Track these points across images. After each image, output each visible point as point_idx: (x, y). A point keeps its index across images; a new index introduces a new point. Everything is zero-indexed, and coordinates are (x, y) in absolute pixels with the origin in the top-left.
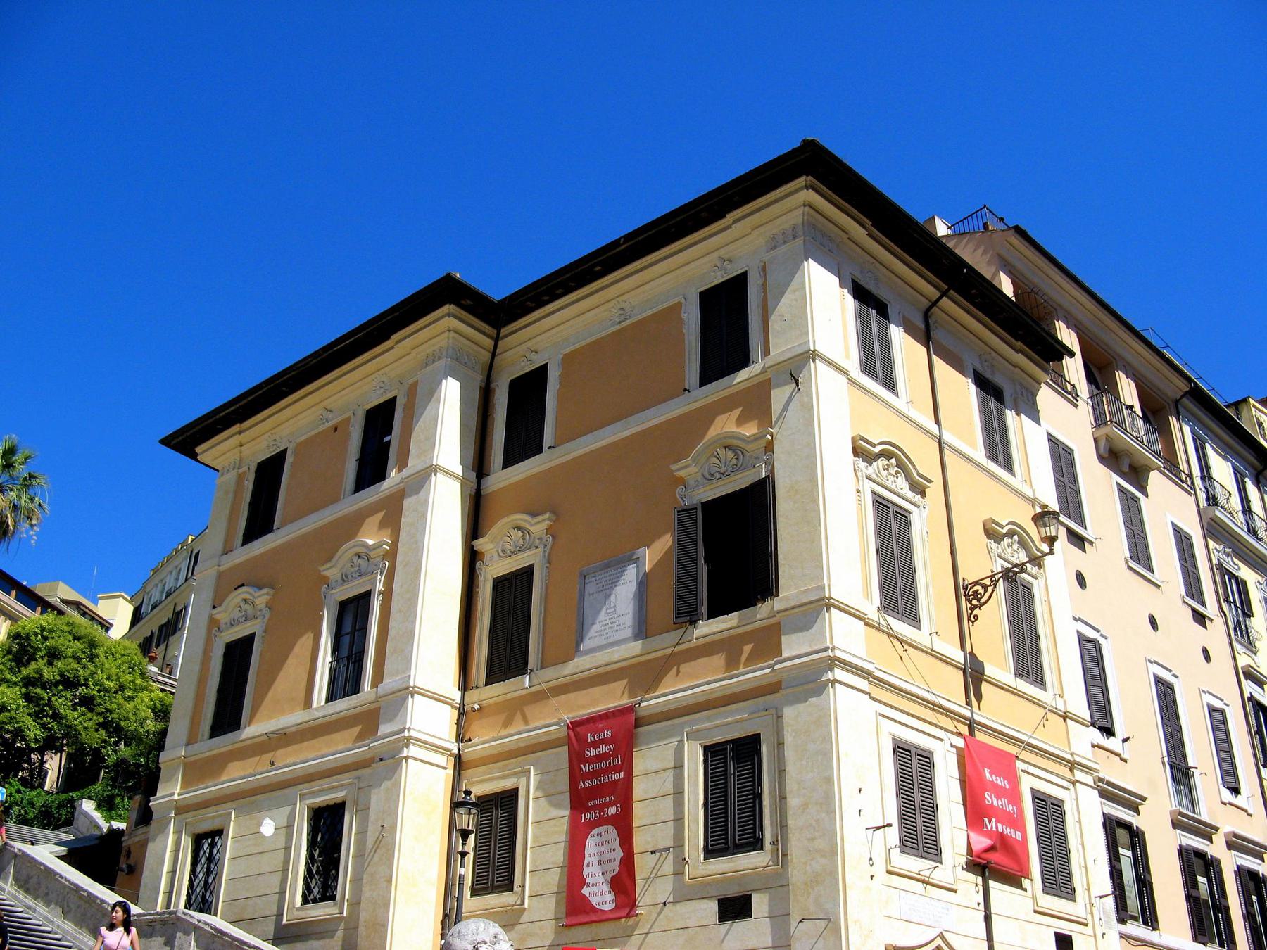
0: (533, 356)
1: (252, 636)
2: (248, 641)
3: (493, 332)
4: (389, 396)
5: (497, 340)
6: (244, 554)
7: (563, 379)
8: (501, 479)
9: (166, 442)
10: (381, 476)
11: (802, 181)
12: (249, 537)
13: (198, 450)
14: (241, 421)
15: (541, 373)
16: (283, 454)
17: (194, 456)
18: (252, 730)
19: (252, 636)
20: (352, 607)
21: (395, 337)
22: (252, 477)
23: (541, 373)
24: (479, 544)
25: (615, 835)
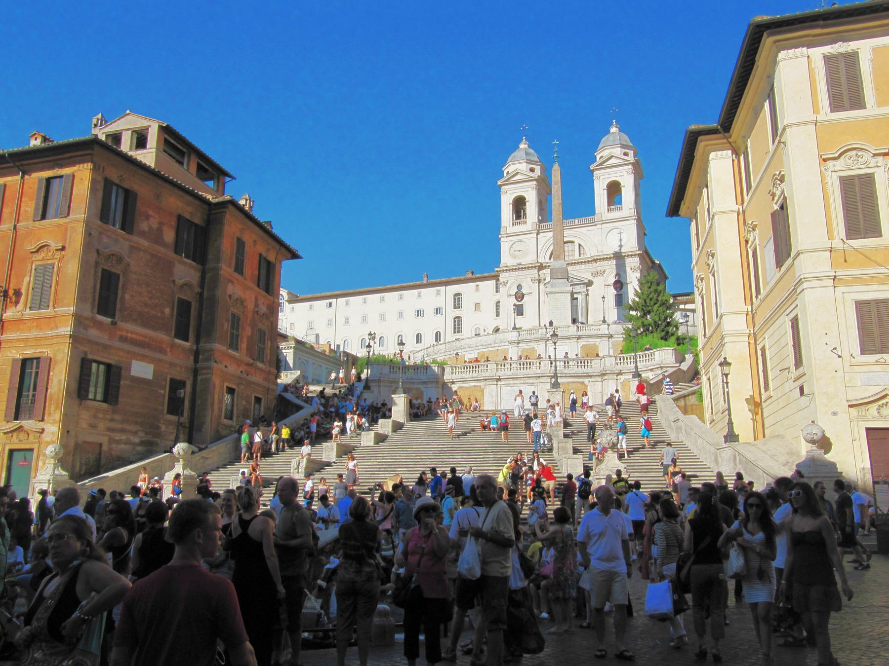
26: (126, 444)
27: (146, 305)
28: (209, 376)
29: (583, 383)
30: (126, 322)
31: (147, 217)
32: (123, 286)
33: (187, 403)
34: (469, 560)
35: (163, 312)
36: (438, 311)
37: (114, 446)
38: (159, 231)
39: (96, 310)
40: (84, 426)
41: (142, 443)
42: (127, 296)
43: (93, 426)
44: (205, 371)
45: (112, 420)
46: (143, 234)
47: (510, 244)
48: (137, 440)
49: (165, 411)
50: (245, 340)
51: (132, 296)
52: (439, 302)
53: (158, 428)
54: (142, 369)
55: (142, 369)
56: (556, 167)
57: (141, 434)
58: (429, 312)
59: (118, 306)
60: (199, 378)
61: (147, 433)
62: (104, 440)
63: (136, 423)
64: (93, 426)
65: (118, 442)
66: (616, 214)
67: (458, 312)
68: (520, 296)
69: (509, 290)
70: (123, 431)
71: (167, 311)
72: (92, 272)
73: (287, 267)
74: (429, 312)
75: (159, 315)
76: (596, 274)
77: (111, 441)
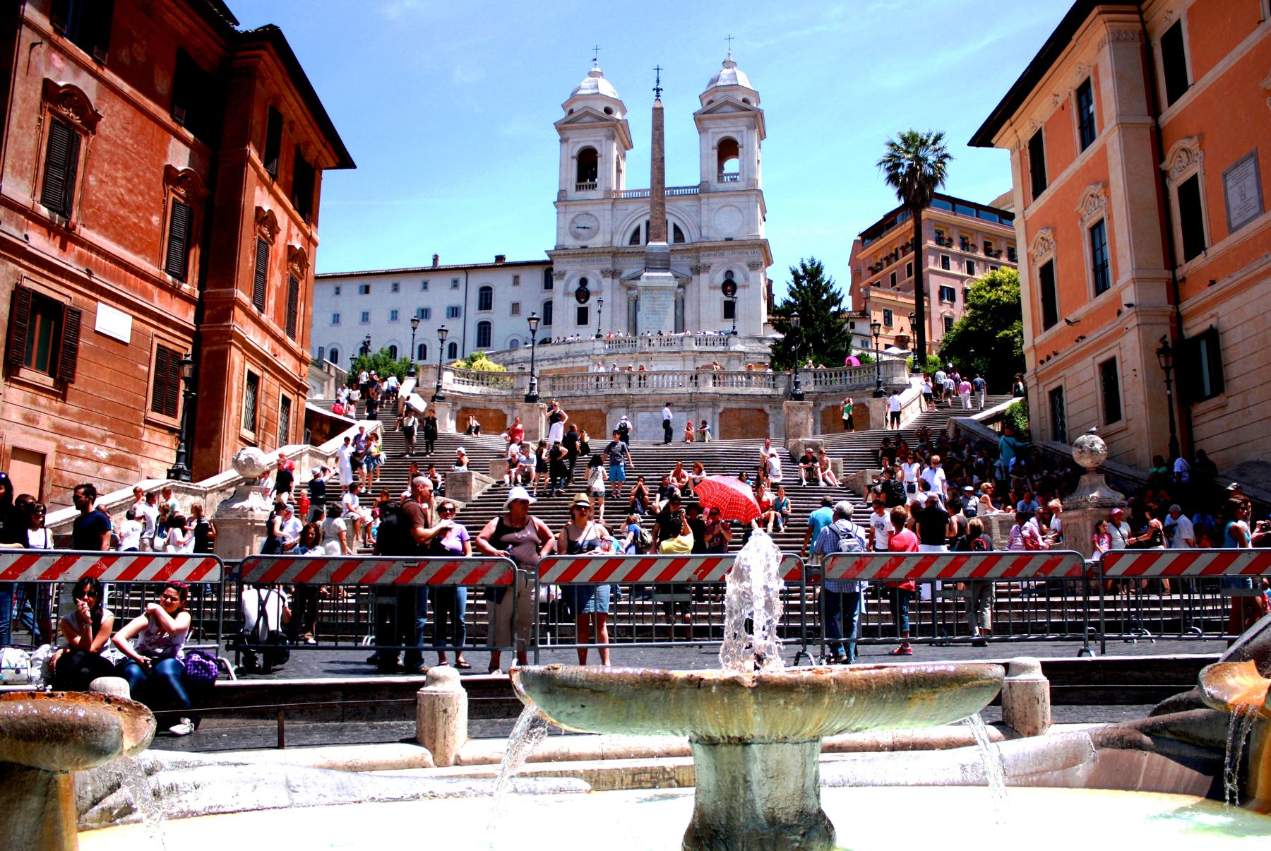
0: (1169, 16)
1: (1196, 176)
2: (1194, 180)
3: (1134, 8)
4: (1085, 77)
5: (1140, 13)
6: (1035, 206)
7: (1190, 29)
8: (1170, 113)
9: (971, 143)
10: (1092, 138)
11: (1095, 11)
12: (1036, 194)
13: (993, 141)
14: (1009, 117)
15: (1177, 26)
16: (1040, 132)
17: (992, 146)
18: (1214, 250)
19: (1195, 177)
20: (1097, 231)
21: (1075, 37)
22: (1028, 152)
23: (1177, 26)
24: (1163, 166)
25: (490, 657)
26: (85, 458)
27: (123, 203)
28: (222, 347)
29: (761, 410)
30: (89, 228)
32: (87, 158)
34: (812, 650)
35: (150, 223)
36: (454, 312)
37: (65, 461)
39: (38, 197)
40: (15, 416)
41: (113, 461)
42: (92, 180)
43: (30, 420)
44: (216, 339)
45: (62, 412)
47: (571, 216)
48: (103, 454)
49: (149, 406)
50: (273, 293)
51: (101, 182)
52: (456, 298)
53: (138, 435)
54: (113, 322)
55: (113, 322)
56: (39, 317)
57: (111, 443)
58: (439, 316)
59: (77, 194)
60: (205, 350)
61: (119, 443)
62: (48, 447)
63: (103, 422)
64: (30, 420)
65: (74, 455)
66: (591, 194)
67: (485, 316)
68: (582, 294)
69: (567, 285)
70: (81, 434)
71: (156, 220)
72: (34, 120)
73: (331, 180)
74: (439, 316)
75: (142, 225)
76: (697, 270)
77: (61, 451)
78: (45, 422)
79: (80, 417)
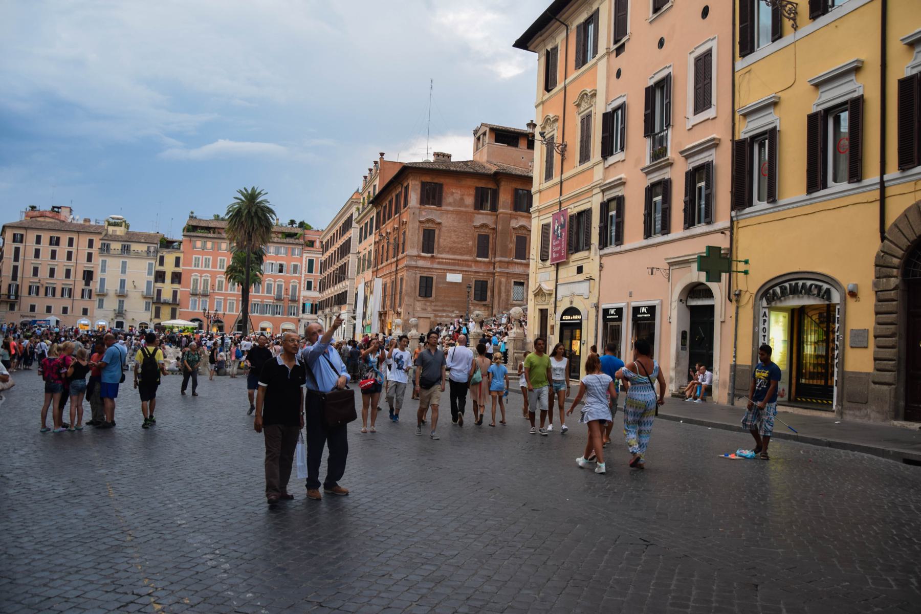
27: (454, 242)
31: (452, 194)
33: (489, 293)
38: (462, 199)
46: (450, 204)
70: (444, 311)
77: (436, 316)
78: (429, 309)
79: (443, 306)
